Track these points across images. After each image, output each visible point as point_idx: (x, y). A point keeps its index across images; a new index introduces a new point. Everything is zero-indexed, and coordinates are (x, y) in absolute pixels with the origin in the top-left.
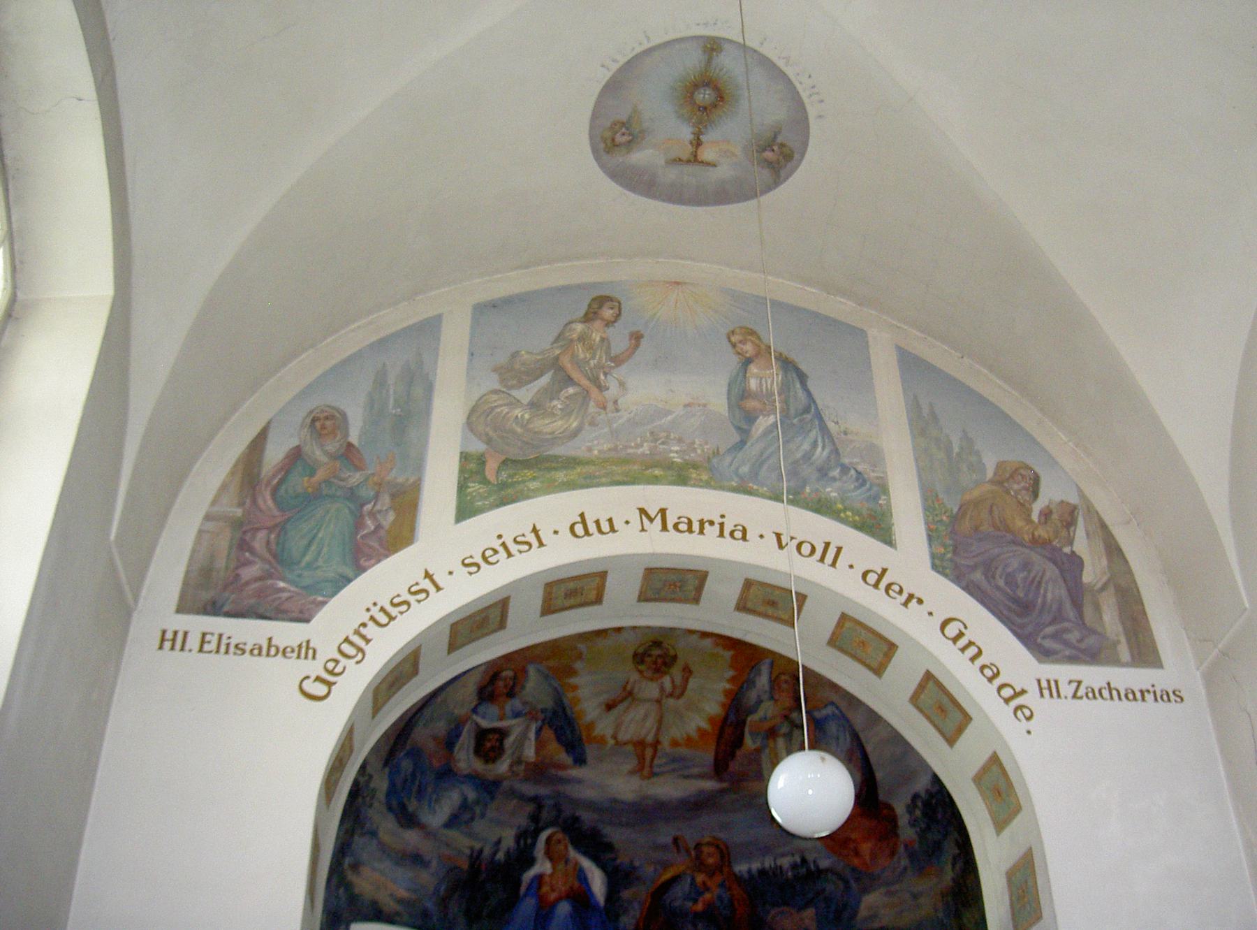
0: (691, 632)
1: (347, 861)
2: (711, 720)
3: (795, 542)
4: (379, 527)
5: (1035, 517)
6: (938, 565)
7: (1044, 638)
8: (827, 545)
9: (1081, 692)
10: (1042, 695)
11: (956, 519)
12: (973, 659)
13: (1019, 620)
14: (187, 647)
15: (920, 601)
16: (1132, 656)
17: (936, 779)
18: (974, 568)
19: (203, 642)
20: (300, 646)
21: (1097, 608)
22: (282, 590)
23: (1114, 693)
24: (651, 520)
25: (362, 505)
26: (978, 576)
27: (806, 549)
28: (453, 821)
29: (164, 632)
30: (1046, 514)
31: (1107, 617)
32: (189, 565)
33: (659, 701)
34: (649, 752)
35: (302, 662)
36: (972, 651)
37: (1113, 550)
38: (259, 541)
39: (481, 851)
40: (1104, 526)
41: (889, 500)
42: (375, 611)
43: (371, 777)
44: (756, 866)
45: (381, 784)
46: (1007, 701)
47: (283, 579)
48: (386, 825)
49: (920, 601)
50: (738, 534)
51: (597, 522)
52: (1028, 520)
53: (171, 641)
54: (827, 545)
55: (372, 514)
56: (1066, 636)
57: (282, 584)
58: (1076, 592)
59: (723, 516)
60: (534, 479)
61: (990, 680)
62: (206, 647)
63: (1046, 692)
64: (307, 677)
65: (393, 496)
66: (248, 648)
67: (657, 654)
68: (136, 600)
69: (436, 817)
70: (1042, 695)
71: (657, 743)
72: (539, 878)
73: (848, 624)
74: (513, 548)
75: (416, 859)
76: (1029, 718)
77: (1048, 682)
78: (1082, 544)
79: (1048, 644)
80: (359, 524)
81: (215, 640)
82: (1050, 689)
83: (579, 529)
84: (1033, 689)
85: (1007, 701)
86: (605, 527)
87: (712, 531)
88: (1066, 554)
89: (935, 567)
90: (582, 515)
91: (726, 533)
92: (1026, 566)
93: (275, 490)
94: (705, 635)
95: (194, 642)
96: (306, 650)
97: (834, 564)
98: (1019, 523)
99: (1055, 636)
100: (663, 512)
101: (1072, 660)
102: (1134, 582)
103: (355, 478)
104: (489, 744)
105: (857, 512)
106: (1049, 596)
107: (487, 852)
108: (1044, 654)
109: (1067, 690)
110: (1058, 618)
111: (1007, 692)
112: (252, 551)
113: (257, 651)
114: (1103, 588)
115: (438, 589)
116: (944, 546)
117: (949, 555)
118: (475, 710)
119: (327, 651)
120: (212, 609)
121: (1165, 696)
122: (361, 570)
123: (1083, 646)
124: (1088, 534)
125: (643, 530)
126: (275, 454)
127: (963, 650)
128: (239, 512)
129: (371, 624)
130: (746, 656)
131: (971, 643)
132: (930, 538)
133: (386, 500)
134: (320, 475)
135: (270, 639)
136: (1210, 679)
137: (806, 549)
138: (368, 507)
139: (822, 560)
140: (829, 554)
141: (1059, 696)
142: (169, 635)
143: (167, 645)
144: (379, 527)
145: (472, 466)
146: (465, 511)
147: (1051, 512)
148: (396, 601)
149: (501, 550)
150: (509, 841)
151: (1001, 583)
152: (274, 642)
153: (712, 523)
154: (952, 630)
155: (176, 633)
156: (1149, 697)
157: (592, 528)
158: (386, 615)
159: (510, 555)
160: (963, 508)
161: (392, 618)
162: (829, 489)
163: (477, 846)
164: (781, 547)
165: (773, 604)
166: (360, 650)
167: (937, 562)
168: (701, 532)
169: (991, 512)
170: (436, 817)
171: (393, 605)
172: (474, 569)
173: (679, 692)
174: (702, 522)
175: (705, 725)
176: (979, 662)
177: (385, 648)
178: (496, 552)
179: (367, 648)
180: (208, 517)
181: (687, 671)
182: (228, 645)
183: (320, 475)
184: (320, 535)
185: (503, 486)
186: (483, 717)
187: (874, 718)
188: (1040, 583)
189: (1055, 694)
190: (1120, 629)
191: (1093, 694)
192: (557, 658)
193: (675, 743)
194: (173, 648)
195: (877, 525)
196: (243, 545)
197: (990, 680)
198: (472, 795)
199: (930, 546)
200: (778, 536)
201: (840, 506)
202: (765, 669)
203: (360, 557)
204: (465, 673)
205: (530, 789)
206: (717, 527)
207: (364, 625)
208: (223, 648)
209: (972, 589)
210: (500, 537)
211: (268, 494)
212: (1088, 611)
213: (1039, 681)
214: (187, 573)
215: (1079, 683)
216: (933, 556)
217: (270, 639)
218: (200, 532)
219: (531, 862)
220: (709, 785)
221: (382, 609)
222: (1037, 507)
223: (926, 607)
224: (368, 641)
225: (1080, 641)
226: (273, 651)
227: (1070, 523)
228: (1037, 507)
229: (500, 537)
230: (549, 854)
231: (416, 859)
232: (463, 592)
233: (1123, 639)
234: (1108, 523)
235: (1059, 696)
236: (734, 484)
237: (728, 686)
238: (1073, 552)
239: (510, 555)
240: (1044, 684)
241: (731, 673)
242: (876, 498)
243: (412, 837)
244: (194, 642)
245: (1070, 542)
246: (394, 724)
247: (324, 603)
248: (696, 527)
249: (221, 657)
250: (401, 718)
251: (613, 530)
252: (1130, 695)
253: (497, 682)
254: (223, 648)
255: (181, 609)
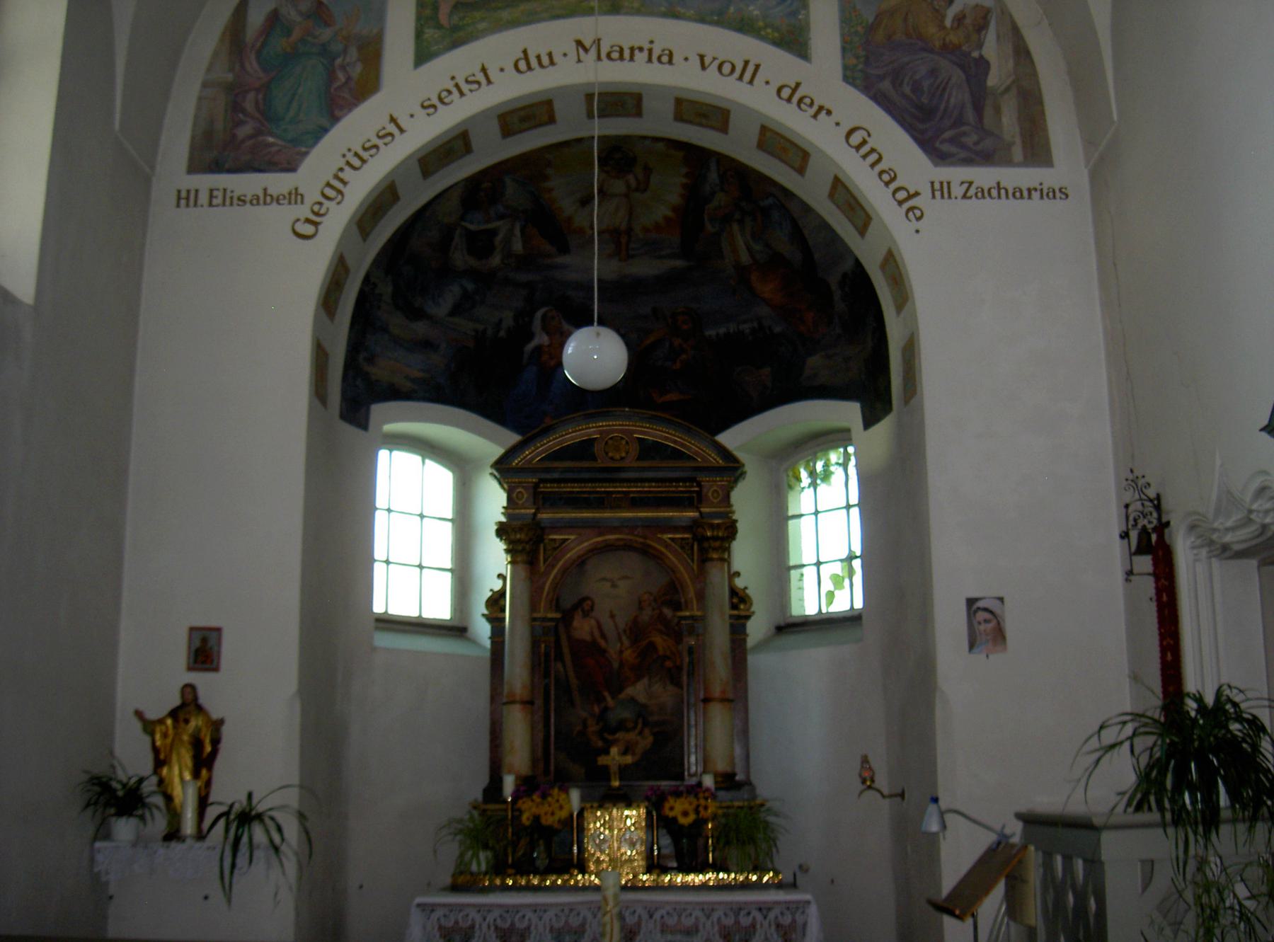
0: (645, 138)
1: (361, 356)
2: (674, 209)
3: (716, 63)
4: (349, 79)
5: (948, 22)
6: (849, 77)
7: (942, 142)
8: (746, 63)
9: (972, 191)
10: (934, 197)
11: (872, 29)
12: (873, 166)
13: (921, 126)
14: (199, 202)
15: (829, 113)
16: (1025, 157)
17: (858, 264)
18: (881, 78)
19: (211, 197)
20: (290, 194)
21: (997, 110)
22: (272, 145)
23: (1003, 192)
24: (586, 50)
25: (334, 59)
26: (886, 85)
27: (727, 68)
28: (456, 311)
29: (179, 192)
30: (959, 19)
31: (1005, 120)
32: (193, 131)
33: (626, 196)
34: (624, 240)
35: (293, 207)
36: (874, 157)
37: (1022, 53)
38: (249, 104)
39: (485, 331)
40: (1015, 30)
41: (808, 15)
42: (350, 157)
43: (375, 285)
44: (722, 331)
45: (386, 289)
46: (900, 203)
47: (271, 134)
48: (397, 322)
49: (829, 113)
50: (665, 59)
51: (538, 57)
52: (942, 27)
53: (186, 199)
54: (746, 63)
55: (343, 68)
56: (964, 139)
57: (271, 140)
58: (980, 97)
59: (652, 42)
60: (483, 19)
61: (887, 184)
62: (215, 202)
63: (938, 194)
64: (298, 220)
65: (360, 48)
66: (248, 199)
67: (619, 155)
68: (153, 168)
69: (441, 308)
70: (934, 197)
71: (629, 230)
72: (539, 349)
73: (768, 134)
74: (465, 88)
75: (427, 345)
76: (918, 219)
77: (941, 183)
78: (992, 48)
79: (946, 148)
80: (331, 76)
81: (220, 194)
82: (942, 190)
83: (522, 65)
84: (927, 192)
85: (900, 203)
86: (545, 61)
87: (641, 57)
88: (975, 59)
89: (846, 79)
90: (525, 52)
91: (654, 58)
92: (933, 72)
93: (259, 53)
94: (656, 140)
95: (203, 198)
96: (295, 196)
97: (751, 82)
98: (932, 30)
99: (952, 141)
100: (598, 42)
101: (968, 162)
102: (1038, 83)
103: (326, 34)
104: (481, 244)
105: (776, 29)
106: (952, 100)
107: (490, 332)
108: (939, 157)
109: (958, 191)
110: (959, 122)
111: (901, 195)
112: (243, 111)
113: (255, 201)
114: (1007, 89)
115: (402, 131)
116: (857, 58)
117: (860, 67)
118: (462, 218)
119: (312, 196)
120: (216, 167)
121: (1052, 194)
122: (335, 119)
123: (979, 148)
124: (998, 37)
125: (579, 61)
126: (256, 19)
127: (864, 157)
128: (230, 77)
129: (347, 168)
130: (696, 157)
131: (873, 150)
132: (844, 50)
133: (353, 53)
134: (296, 34)
135: (265, 190)
136: (1095, 177)
137: (727, 68)
138: (339, 61)
139: (741, 78)
140: (748, 72)
141: (950, 197)
142: (184, 194)
143: (183, 202)
144: (349, 79)
145: (428, 12)
146: (422, 56)
147: (964, 17)
148: (367, 145)
149: (454, 90)
150: (508, 318)
151: (907, 89)
152: (269, 192)
153: (641, 49)
154: (856, 138)
155: (188, 191)
156: (1036, 195)
157: (534, 62)
158: (358, 160)
159: (462, 94)
160: (878, 17)
161: (364, 161)
162: (751, 8)
163: (481, 327)
164: (703, 67)
165: (705, 116)
166: (340, 192)
167: (848, 73)
168: (632, 59)
169: (905, 20)
170: (441, 308)
171: (365, 149)
172: (432, 110)
173: (643, 187)
174: (632, 49)
175: (669, 213)
176: (878, 168)
177: (361, 187)
178: (450, 92)
179: (345, 190)
180: (205, 85)
181: (648, 170)
182: (232, 198)
183: (296, 34)
184: (300, 91)
185: (455, 28)
186: (472, 223)
187: (807, 208)
188: (944, 89)
189: (946, 195)
190: (1017, 129)
191: (983, 194)
192: (530, 167)
193: (646, 230)
194: (188, 205)
195: (794, 41)
196: (236, 107)
197: (887, 184)
198: (470, 286)
199: (843, 57)
200: (702, 57)
201: (761, 24)
202: (713, 166)
203: (335, 105)
204: (452, 187)
205: (522, 277)
206: (646, 53)
207: (341, 170)
208: (228, 202)
209: (881, 99)
210: (453, 78)
211: (253, 57)
212: (988, 112)
213: (932, 183)
214: (193, 138)
215: (971, 184)
216: (846, 68)
217: (265, 190)
218: (200, 99)
219: (531, 336)
220: (679, 263)
221: (356, 155)
222: (951, 13)
223: (834, 118)
224: (345, 183)
225: (976, 144)
226: (268, 199)
227: (981, 27)
228: (951, 13)
229: (453, 78)
230: (545, 328)
231: (427, 345)
232: (424, 131)
233: (1018, 140)
234: (1020, 24)
235: (950, 197)
236: (663, 9)
237: (684, 181)
238: (981, 57)
239: (462, 94)
240: (937, 186)
241: (684, 170)
242: (794, 14)
243: (421, 328)
244: (203, 198)
245: (980, 46)
246: (389, 241)
247: (306, 154)
248: (627, 54)
249: (227, 209)
250: (394, 235)
251: (552, 63)
252: (1018, 194)
253: (479, 191)
254: (228, 202)
255: (193, 168)
